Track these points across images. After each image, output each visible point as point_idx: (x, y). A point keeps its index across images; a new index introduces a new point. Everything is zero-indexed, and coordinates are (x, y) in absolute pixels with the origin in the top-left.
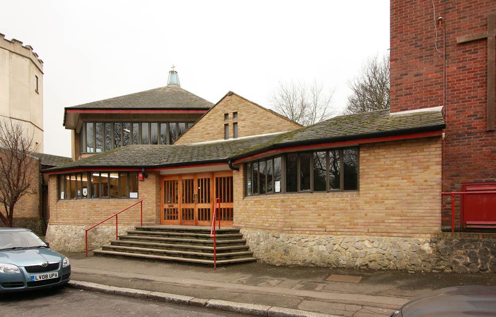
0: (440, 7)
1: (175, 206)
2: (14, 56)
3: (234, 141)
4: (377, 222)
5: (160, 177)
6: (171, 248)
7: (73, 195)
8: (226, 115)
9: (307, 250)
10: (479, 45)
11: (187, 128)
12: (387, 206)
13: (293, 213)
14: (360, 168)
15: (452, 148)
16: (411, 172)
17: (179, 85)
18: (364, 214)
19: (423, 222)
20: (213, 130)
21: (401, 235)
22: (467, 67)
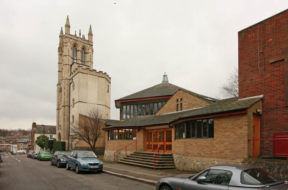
0: (262, 46)
1: (151, 143)
2: (100, 78)
3: (181, 112)
4: (221, 152)
5: (145, 130)
6: (143, 161)
7: (112, 138)
8: (178, 100)
9: (192, 164)
10: (281, 63)
11: (162, 106)
12: (225, 145)
13: (188, 147)
14: (214, 127)
15: (268, 116)
16: (235, 129)
17: (168, 82)
18: (215, 149)
19: (240, 153)
20: (172, 107)
21: (230, 159)
22: (275, 75)
